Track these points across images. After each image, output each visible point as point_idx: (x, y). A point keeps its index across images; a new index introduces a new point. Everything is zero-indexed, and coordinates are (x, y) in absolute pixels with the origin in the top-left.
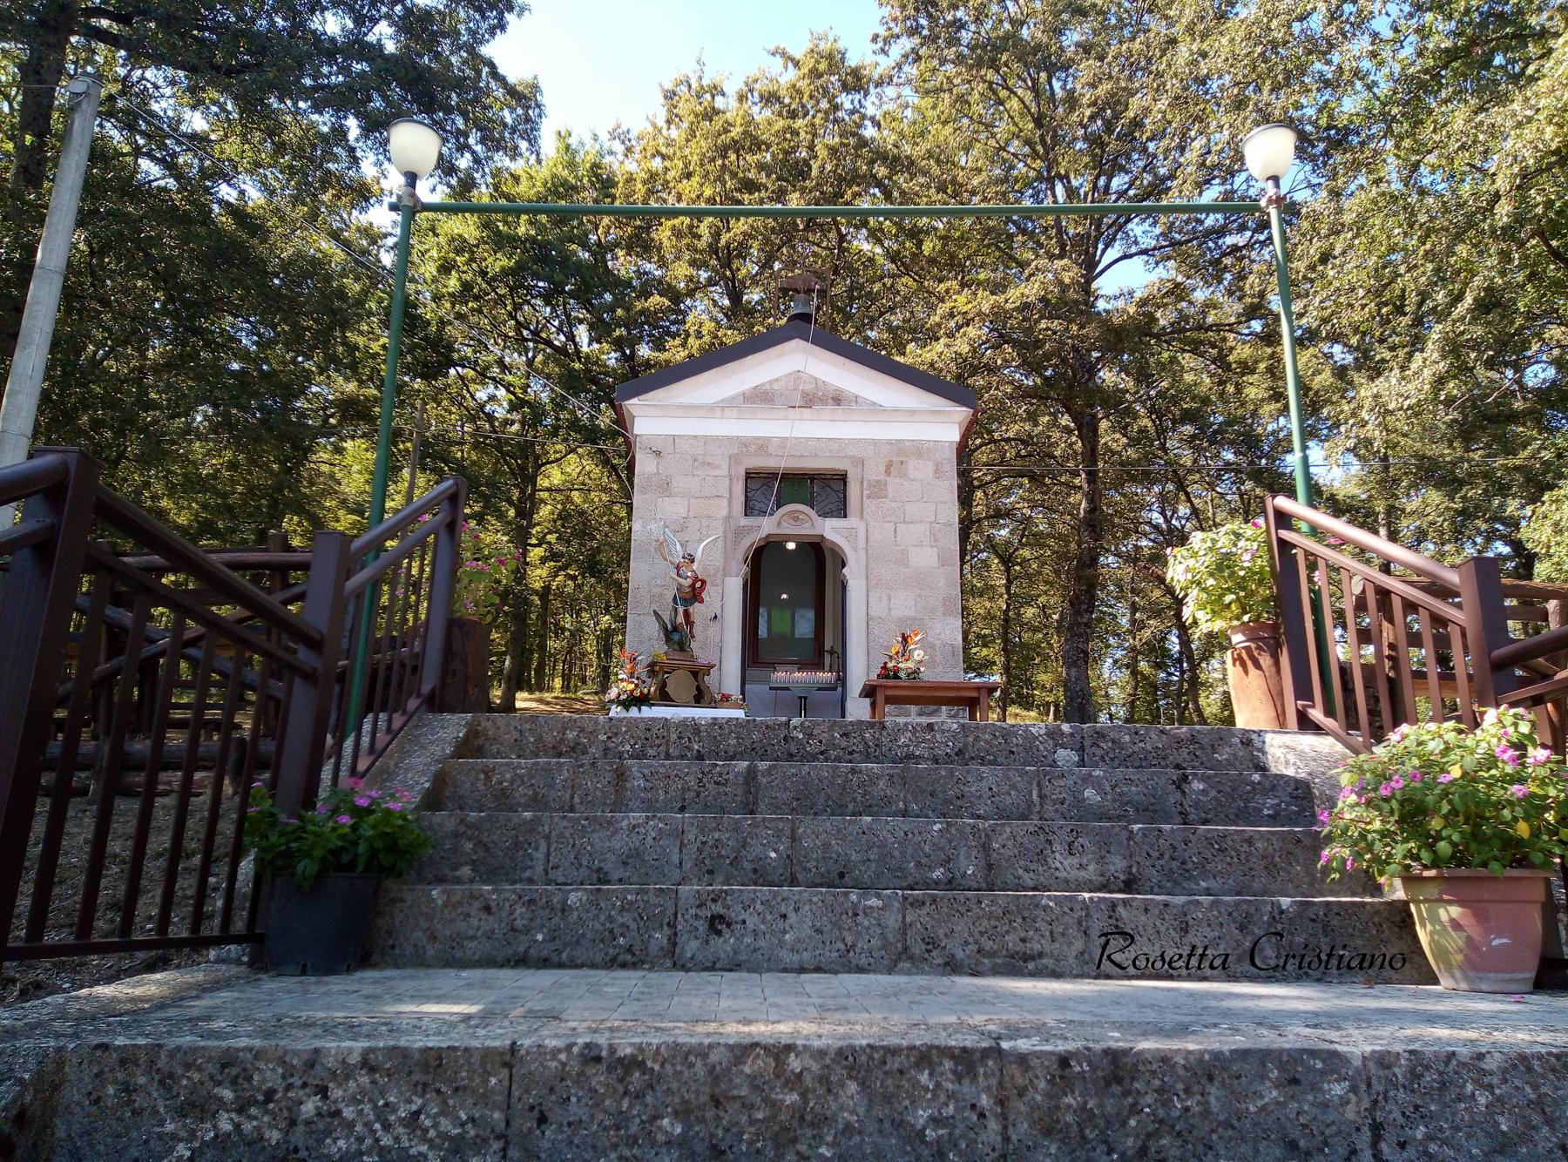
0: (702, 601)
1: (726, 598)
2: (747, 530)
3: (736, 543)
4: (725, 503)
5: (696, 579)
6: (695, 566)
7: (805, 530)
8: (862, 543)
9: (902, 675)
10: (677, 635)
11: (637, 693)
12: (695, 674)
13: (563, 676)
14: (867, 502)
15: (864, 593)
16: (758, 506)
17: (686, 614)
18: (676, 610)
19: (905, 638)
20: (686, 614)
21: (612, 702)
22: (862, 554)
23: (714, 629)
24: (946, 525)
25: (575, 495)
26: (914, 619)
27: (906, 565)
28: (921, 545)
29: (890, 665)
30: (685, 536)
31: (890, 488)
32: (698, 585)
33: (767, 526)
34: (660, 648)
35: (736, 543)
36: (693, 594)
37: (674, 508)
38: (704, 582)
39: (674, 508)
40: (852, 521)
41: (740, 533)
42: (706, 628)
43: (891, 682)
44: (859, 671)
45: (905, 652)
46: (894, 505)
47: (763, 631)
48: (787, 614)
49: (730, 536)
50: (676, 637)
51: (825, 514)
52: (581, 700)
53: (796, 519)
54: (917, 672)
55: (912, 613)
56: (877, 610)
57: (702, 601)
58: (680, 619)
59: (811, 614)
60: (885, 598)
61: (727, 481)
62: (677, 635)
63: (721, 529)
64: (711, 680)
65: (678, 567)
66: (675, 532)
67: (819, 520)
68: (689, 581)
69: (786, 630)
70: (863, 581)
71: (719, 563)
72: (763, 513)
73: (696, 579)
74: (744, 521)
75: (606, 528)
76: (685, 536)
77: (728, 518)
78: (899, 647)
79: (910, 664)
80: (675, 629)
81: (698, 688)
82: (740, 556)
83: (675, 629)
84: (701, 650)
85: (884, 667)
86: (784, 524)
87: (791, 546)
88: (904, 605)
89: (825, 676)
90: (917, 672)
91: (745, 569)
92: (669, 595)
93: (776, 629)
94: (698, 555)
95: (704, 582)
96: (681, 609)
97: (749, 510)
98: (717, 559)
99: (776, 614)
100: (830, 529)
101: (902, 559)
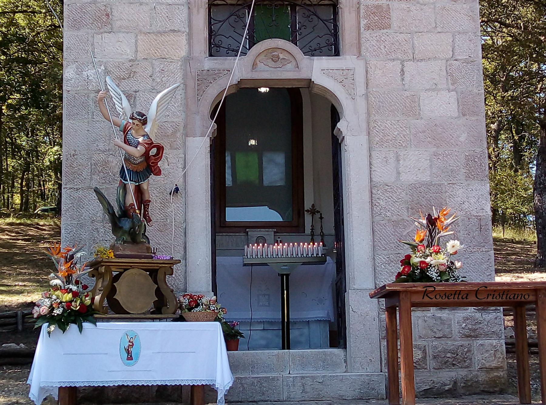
0: (158, 173)
1: (190, 163)
2: (214, 75)
3: (200, 91)
4: (183, 40)
5: (150, 145)
6: (147, 129)
7: (287, 73)
8: (361, 89)
9: (433, 274)
10: (128, 222)
11: (76, 306)
12: (153, 273)
13: (22, 193)
14: (366, 34)
15: (365, 152)
16: (226, 42)
17: (139, 191)
18: (125, 188)
19: (432, 222)
20: (139, 191)
21: (42, 317)
22: (361, 104)
23: (174, 206)
24: (466, 61)
25: (20, 19)
26: (428, 185)
27: (418, 116)
28: (435, 88)
29: (415, 260)
30: (130, 85)
31: (395, 15)
32: (154, 151)
33: (239, 69)
34: (104, 238)
35: (200, 91)
36: (148, 165)
37: (117, 47)
38: (160, 149)
39: (117, 47)
40: (347, 61)
41: (204, 79)
42: (164, 204)
43: (419, 286)
44: (367, 266)
45: (432, 241)
46: (401, 37)
47: (229, 182)
48: (253, 159)
49: (191, 83)
50: (126, 225)
51: (312, 51)
52: (37, 226)
53: (276, 59)
54: (451, 268)
55: (425, 177)
56: (384, 174)
57: (158, 173)
58: (131, 199)
59: (280, 158)
60: (392, 161)
61: (186, 10)
62: (128, 222)
63: (179, 76)
64: (173, 281)
65: (125, 131)
66: (119, 80)
67: (304, 60)
68: (141, 149)
69: (253, 176)
70: (364, 138)
71: (179, 119)
72: (234, 52)
73: (150, 145)
74: (209, 64)
75: (54, 49)
76: (130, 85)
77: (188, 59)
78: (423, 233)
79: (442, 259)
80: (125, 212)
81: (158, 292)
82: (206, 109)
83: (125, 212)
84: (160, 240)
85: (406, 261)
86: (261, 66)
87: (263, 90)
88: (416, 166)
89: (310, 248)
90: (451, 268)
91: (212, 125)
92: (116, 163)
93: (242, 176)
94: (152, 112)
95: (160, 149)
96: (131, 186)
97: (214, 48)
98: (177, 116)
99: (241, 159)
100: (320, 71)
101: (412, 108)
